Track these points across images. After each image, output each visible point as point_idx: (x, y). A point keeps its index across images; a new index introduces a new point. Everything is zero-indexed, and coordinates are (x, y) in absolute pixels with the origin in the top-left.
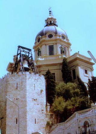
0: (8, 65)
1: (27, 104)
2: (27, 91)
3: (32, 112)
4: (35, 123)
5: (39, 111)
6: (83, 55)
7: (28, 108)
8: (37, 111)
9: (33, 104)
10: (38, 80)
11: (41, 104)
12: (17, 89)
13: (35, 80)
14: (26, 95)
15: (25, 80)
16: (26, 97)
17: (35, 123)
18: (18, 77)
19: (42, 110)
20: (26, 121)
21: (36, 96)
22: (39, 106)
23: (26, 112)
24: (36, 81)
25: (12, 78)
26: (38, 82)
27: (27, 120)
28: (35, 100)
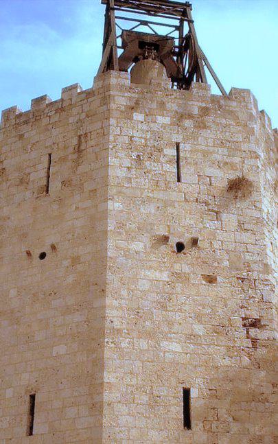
0: (195, 34)
1: (110, 276)
2: (112, 191)
3: (150, 335)
4: (187, 423)
5: (220, 329)
6: (103, 18)
7: (115, 311)
8: (199, 329)
9: (165, 276)
10: (209, 119)
11: (243, 280)
12: (47, 191)
13: (181, 117)
14: (105, 215)
15: (99, 124)
16: (105, 232)
17: (187, 423)
18: (56, 118)
19: (255, 324)
20: (96, 408)
21: (186, 224)
22: (224, 287)
23: (101, 332)
24: (188, 123)
25: (21, 136)
26: (205, 133)
27: (107, 396)
28: (180, 247)
